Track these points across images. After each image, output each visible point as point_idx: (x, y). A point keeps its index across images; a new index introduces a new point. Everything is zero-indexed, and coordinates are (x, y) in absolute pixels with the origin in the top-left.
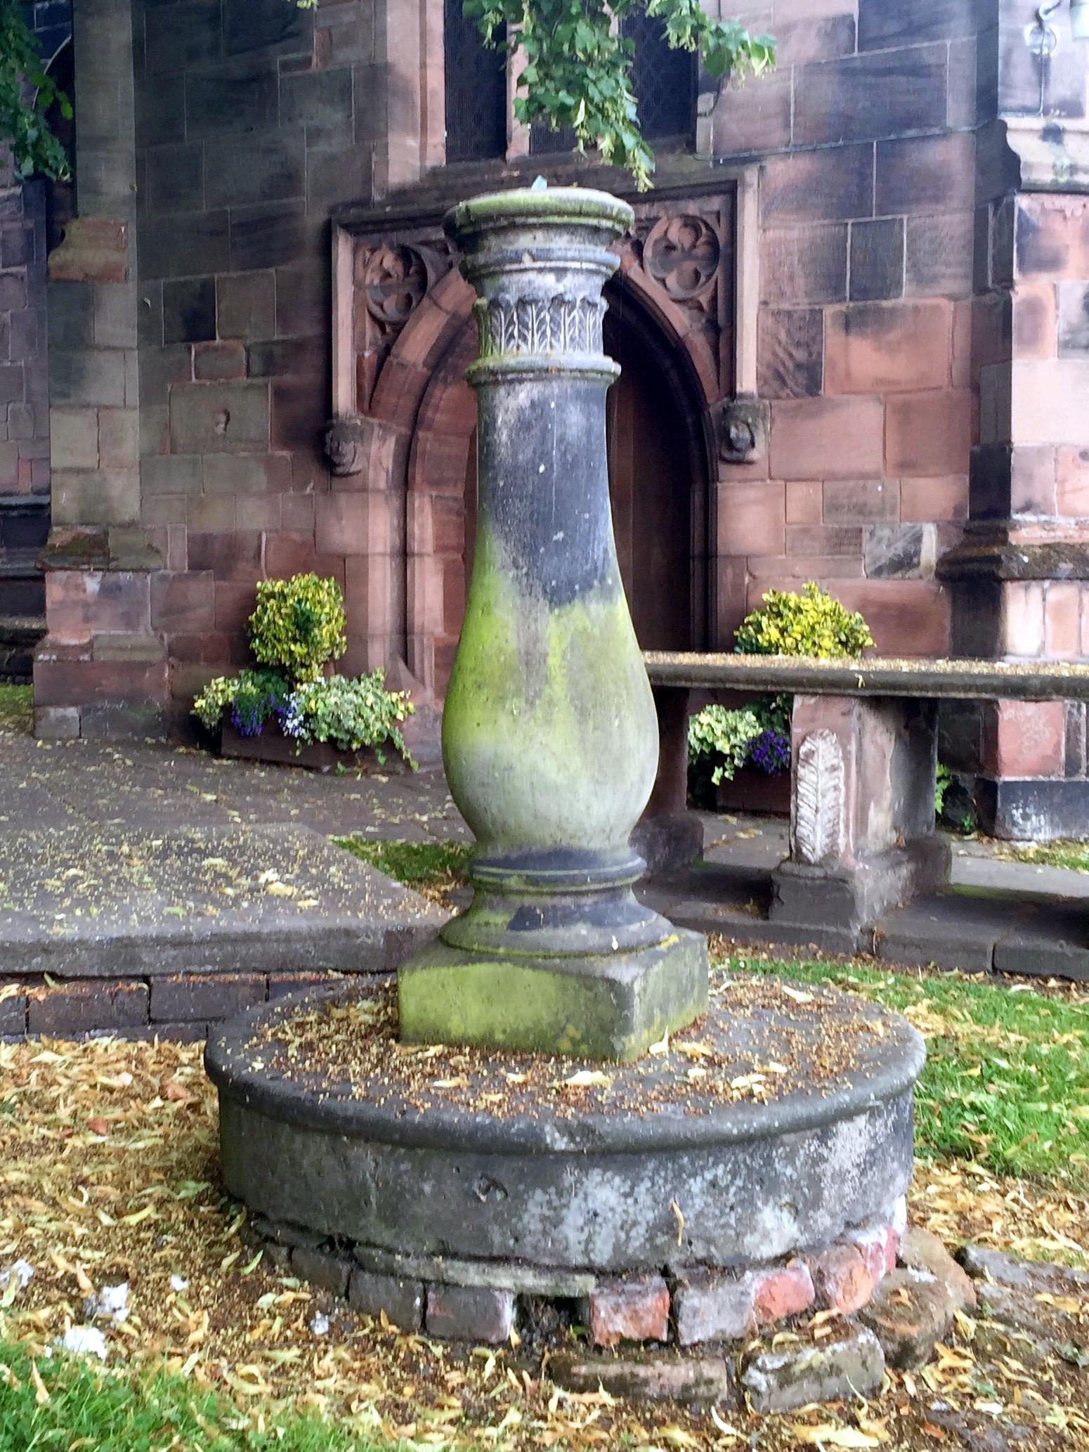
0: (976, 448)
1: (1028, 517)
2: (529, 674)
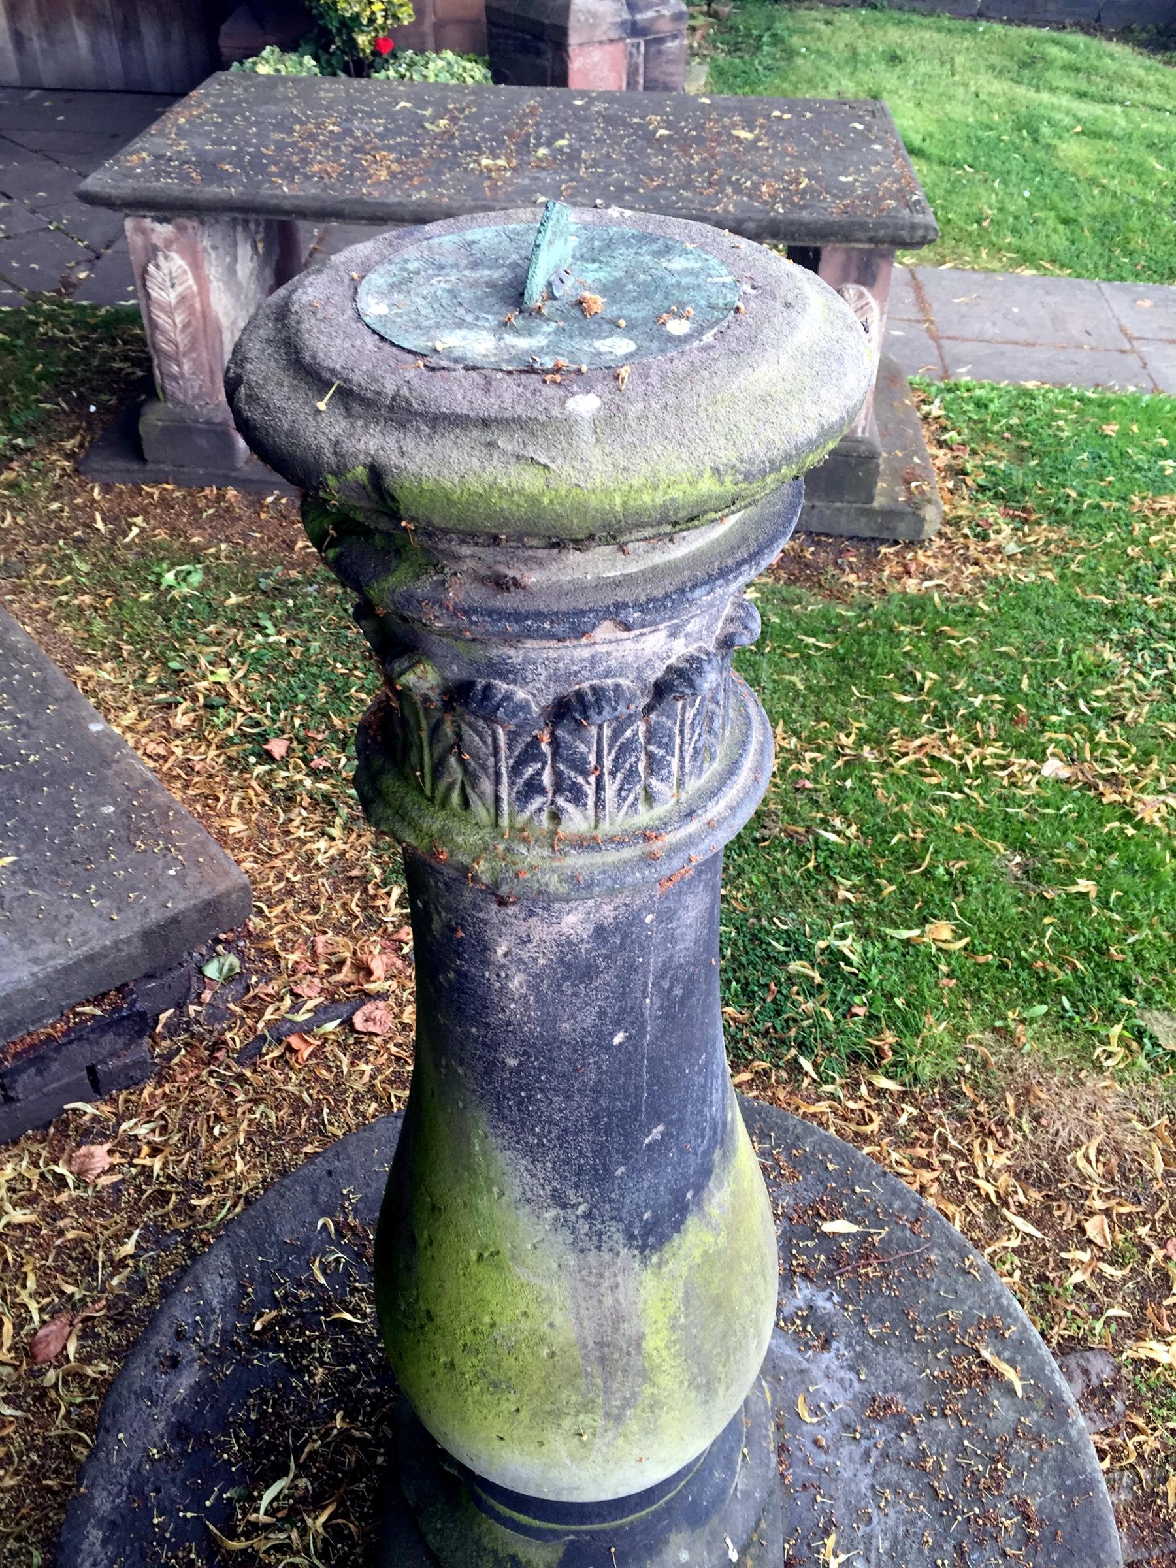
2: (608, 1376)
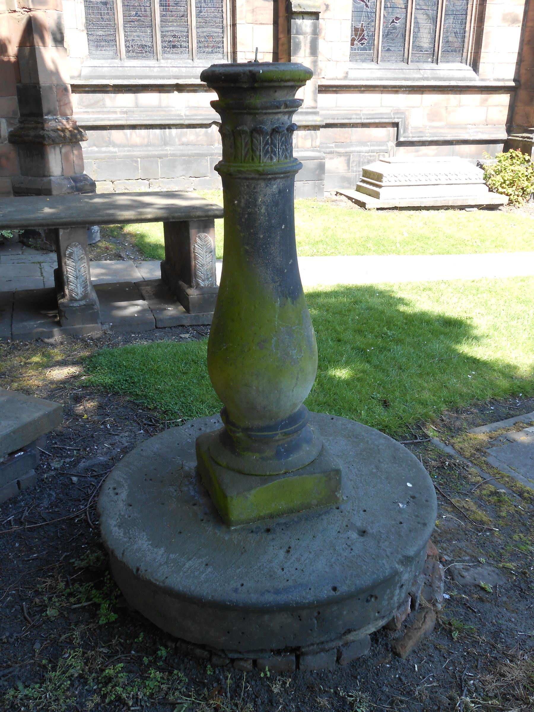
0: (19, 84)
1: (50, 117)
